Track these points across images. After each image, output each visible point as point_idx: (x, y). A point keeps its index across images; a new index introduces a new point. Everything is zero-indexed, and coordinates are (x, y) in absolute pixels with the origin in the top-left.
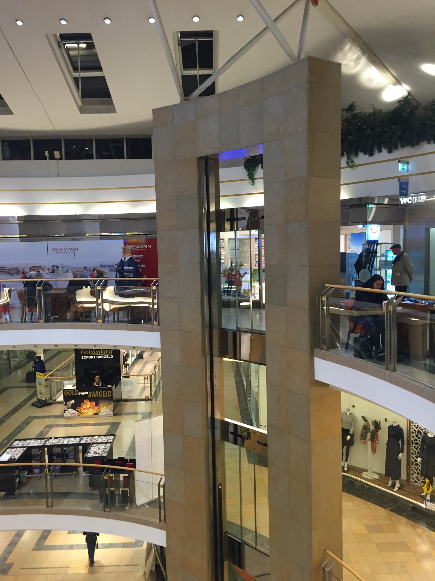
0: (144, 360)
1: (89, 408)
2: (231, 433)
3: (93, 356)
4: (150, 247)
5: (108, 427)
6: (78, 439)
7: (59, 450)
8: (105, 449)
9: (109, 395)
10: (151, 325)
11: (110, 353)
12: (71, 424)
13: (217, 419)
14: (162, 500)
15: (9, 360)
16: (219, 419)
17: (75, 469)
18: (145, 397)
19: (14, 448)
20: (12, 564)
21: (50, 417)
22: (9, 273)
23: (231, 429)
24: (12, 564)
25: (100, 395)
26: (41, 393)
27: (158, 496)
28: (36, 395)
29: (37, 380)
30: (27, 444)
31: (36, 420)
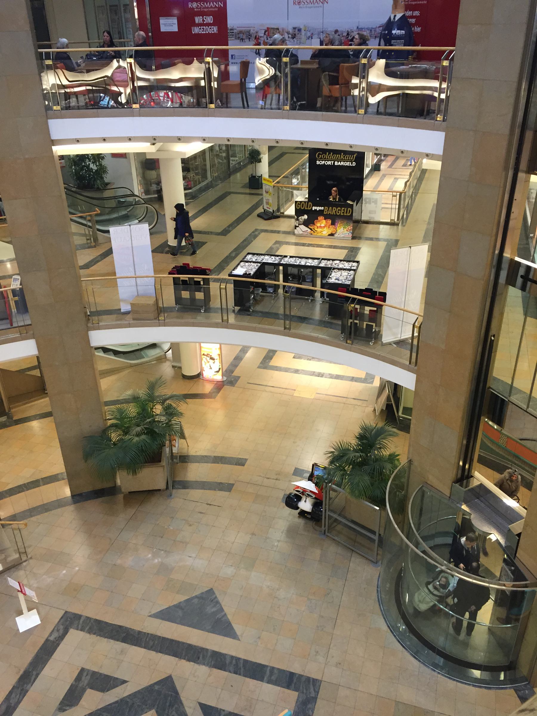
0: (381, 173)
1: (324, 227)
2: (522, 277)
3: (331, 161)
4: (222, 6)
5: (345, 252)
6: (316, 261)
7: (295, 271)
8: (348, 277)
9: (349, 213)
10: (432, 121)
11: (352, 159)
12: (303, 243)
13: (506, 257)
14: (415, 342)
15: (228, 158)
16: (508, 258)
17: (311, 293)
18: (391, 220)
19: (247, 262)
20: (239, 377)
21: (278, 232)
22: (239, 38)
23: (522, 272)
24: (239, 377)
25: (338, 213)
26: (267, 203)
27: (411, 336)
28: (262, 203)
29: (264, 187)
30: (261, 259)
31: (263, 234)
